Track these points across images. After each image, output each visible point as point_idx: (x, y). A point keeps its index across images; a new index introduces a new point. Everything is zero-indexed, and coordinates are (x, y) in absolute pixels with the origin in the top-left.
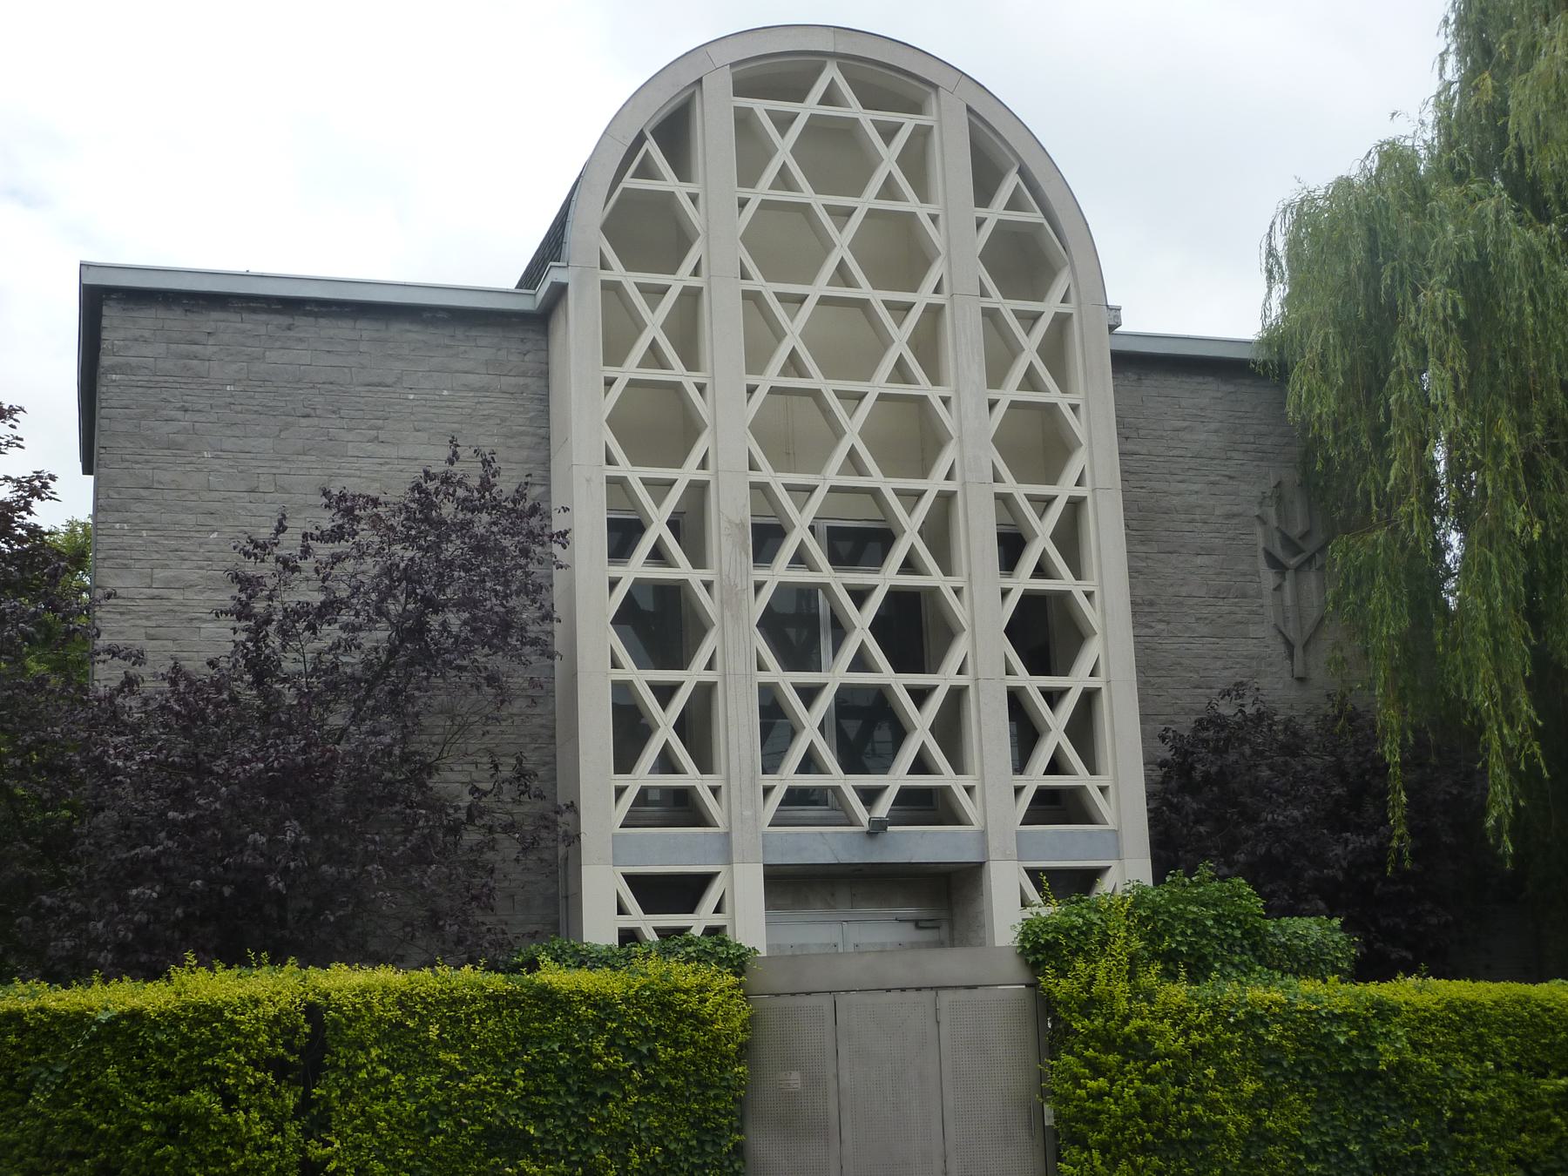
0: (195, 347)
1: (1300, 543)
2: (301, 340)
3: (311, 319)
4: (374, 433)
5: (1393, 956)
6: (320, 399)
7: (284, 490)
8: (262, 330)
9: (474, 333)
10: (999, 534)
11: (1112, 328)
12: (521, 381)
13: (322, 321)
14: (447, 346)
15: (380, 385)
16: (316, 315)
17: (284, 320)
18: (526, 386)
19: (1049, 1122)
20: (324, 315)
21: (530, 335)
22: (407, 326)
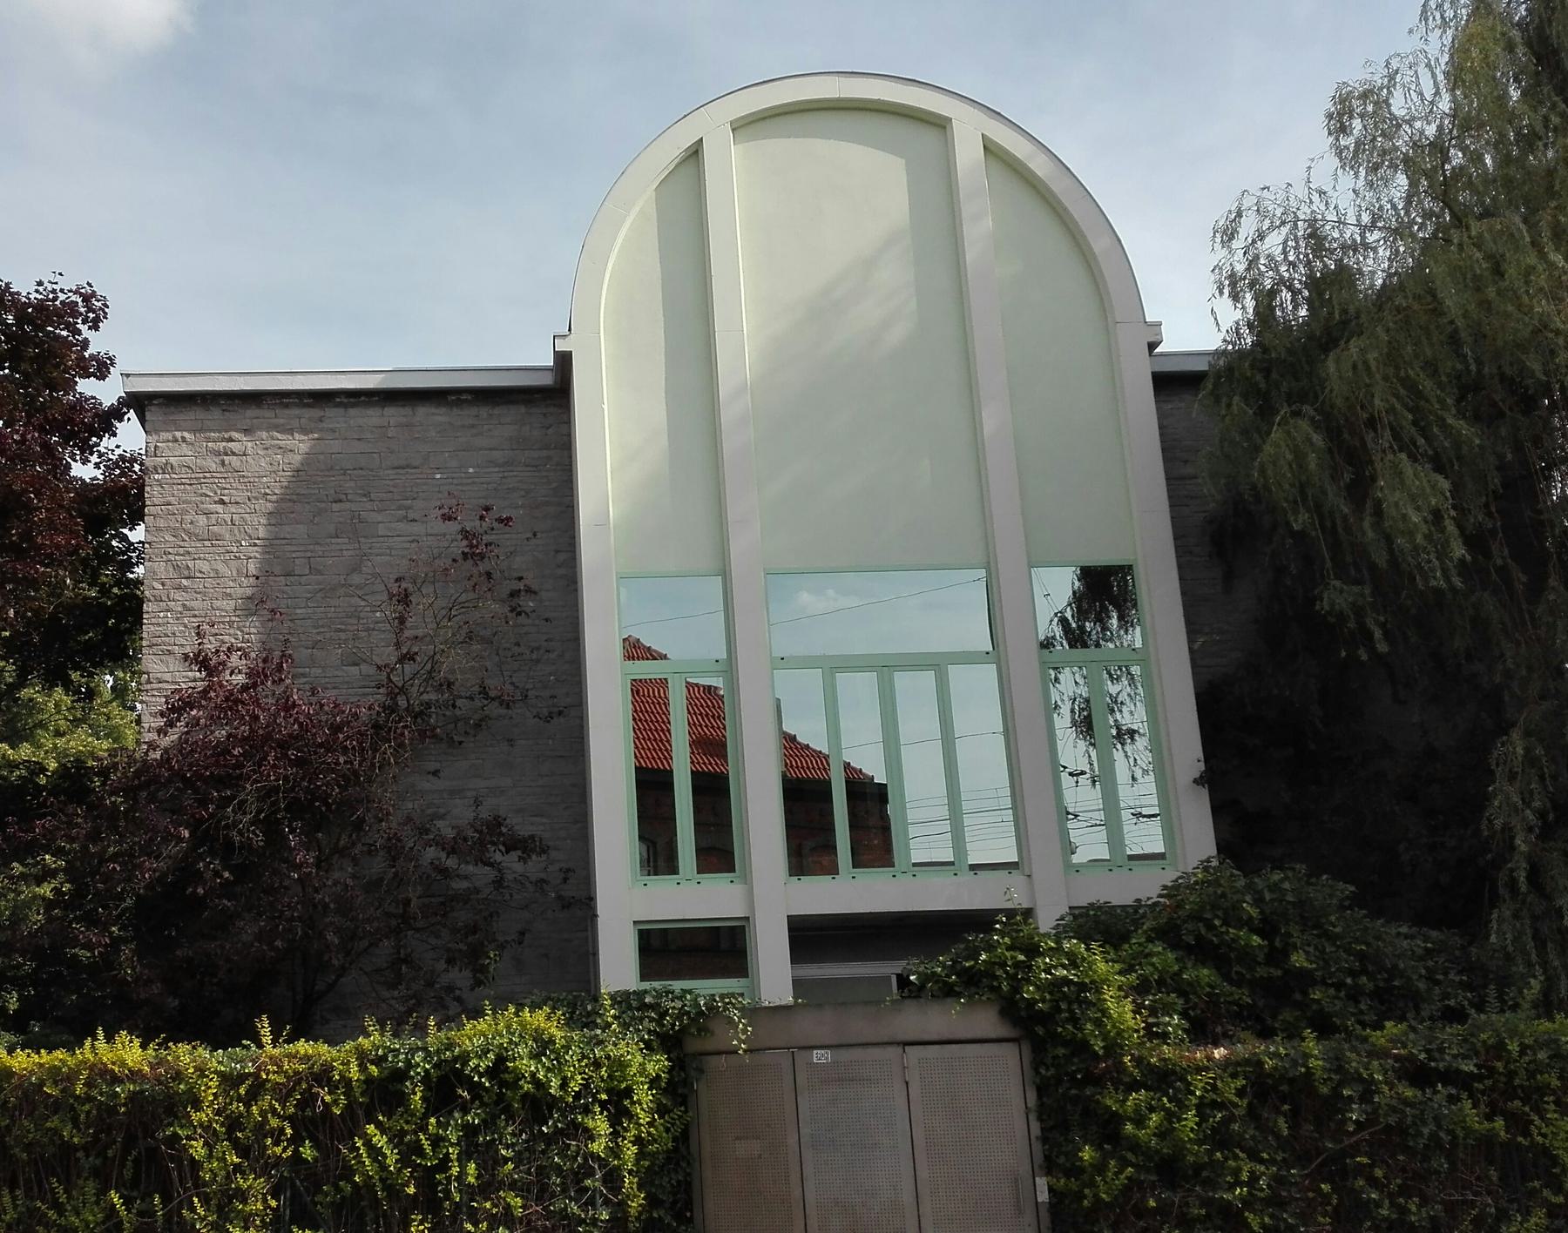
0: (231, 445)
1: (1126, 815)
2: (333, 430)
3: (341, 411)
4: (402, 513)
5: (1524, 579)
6: (352, 484)
7: (320, 573)
8: (295, 423)
9: (497, 411)
10: (639, 770)
11: (1152, 346)
12: (545, 453)
13: (352, 412)
14: (473, 426)
15: (408, 466)
16: (346, 406)
17: (315, 413)
18: (549, 458)
19: (1043, 1196)
20: (353, 405)
21: (552, 409)
22: (433, 410)
